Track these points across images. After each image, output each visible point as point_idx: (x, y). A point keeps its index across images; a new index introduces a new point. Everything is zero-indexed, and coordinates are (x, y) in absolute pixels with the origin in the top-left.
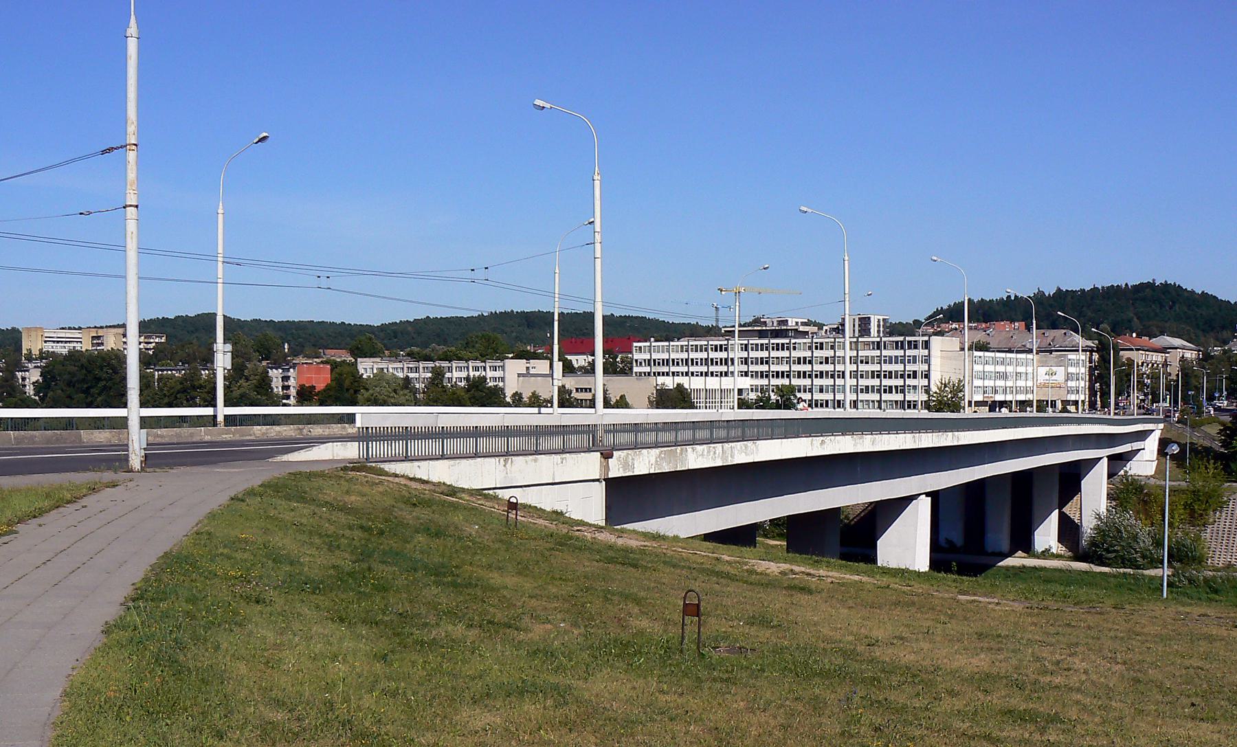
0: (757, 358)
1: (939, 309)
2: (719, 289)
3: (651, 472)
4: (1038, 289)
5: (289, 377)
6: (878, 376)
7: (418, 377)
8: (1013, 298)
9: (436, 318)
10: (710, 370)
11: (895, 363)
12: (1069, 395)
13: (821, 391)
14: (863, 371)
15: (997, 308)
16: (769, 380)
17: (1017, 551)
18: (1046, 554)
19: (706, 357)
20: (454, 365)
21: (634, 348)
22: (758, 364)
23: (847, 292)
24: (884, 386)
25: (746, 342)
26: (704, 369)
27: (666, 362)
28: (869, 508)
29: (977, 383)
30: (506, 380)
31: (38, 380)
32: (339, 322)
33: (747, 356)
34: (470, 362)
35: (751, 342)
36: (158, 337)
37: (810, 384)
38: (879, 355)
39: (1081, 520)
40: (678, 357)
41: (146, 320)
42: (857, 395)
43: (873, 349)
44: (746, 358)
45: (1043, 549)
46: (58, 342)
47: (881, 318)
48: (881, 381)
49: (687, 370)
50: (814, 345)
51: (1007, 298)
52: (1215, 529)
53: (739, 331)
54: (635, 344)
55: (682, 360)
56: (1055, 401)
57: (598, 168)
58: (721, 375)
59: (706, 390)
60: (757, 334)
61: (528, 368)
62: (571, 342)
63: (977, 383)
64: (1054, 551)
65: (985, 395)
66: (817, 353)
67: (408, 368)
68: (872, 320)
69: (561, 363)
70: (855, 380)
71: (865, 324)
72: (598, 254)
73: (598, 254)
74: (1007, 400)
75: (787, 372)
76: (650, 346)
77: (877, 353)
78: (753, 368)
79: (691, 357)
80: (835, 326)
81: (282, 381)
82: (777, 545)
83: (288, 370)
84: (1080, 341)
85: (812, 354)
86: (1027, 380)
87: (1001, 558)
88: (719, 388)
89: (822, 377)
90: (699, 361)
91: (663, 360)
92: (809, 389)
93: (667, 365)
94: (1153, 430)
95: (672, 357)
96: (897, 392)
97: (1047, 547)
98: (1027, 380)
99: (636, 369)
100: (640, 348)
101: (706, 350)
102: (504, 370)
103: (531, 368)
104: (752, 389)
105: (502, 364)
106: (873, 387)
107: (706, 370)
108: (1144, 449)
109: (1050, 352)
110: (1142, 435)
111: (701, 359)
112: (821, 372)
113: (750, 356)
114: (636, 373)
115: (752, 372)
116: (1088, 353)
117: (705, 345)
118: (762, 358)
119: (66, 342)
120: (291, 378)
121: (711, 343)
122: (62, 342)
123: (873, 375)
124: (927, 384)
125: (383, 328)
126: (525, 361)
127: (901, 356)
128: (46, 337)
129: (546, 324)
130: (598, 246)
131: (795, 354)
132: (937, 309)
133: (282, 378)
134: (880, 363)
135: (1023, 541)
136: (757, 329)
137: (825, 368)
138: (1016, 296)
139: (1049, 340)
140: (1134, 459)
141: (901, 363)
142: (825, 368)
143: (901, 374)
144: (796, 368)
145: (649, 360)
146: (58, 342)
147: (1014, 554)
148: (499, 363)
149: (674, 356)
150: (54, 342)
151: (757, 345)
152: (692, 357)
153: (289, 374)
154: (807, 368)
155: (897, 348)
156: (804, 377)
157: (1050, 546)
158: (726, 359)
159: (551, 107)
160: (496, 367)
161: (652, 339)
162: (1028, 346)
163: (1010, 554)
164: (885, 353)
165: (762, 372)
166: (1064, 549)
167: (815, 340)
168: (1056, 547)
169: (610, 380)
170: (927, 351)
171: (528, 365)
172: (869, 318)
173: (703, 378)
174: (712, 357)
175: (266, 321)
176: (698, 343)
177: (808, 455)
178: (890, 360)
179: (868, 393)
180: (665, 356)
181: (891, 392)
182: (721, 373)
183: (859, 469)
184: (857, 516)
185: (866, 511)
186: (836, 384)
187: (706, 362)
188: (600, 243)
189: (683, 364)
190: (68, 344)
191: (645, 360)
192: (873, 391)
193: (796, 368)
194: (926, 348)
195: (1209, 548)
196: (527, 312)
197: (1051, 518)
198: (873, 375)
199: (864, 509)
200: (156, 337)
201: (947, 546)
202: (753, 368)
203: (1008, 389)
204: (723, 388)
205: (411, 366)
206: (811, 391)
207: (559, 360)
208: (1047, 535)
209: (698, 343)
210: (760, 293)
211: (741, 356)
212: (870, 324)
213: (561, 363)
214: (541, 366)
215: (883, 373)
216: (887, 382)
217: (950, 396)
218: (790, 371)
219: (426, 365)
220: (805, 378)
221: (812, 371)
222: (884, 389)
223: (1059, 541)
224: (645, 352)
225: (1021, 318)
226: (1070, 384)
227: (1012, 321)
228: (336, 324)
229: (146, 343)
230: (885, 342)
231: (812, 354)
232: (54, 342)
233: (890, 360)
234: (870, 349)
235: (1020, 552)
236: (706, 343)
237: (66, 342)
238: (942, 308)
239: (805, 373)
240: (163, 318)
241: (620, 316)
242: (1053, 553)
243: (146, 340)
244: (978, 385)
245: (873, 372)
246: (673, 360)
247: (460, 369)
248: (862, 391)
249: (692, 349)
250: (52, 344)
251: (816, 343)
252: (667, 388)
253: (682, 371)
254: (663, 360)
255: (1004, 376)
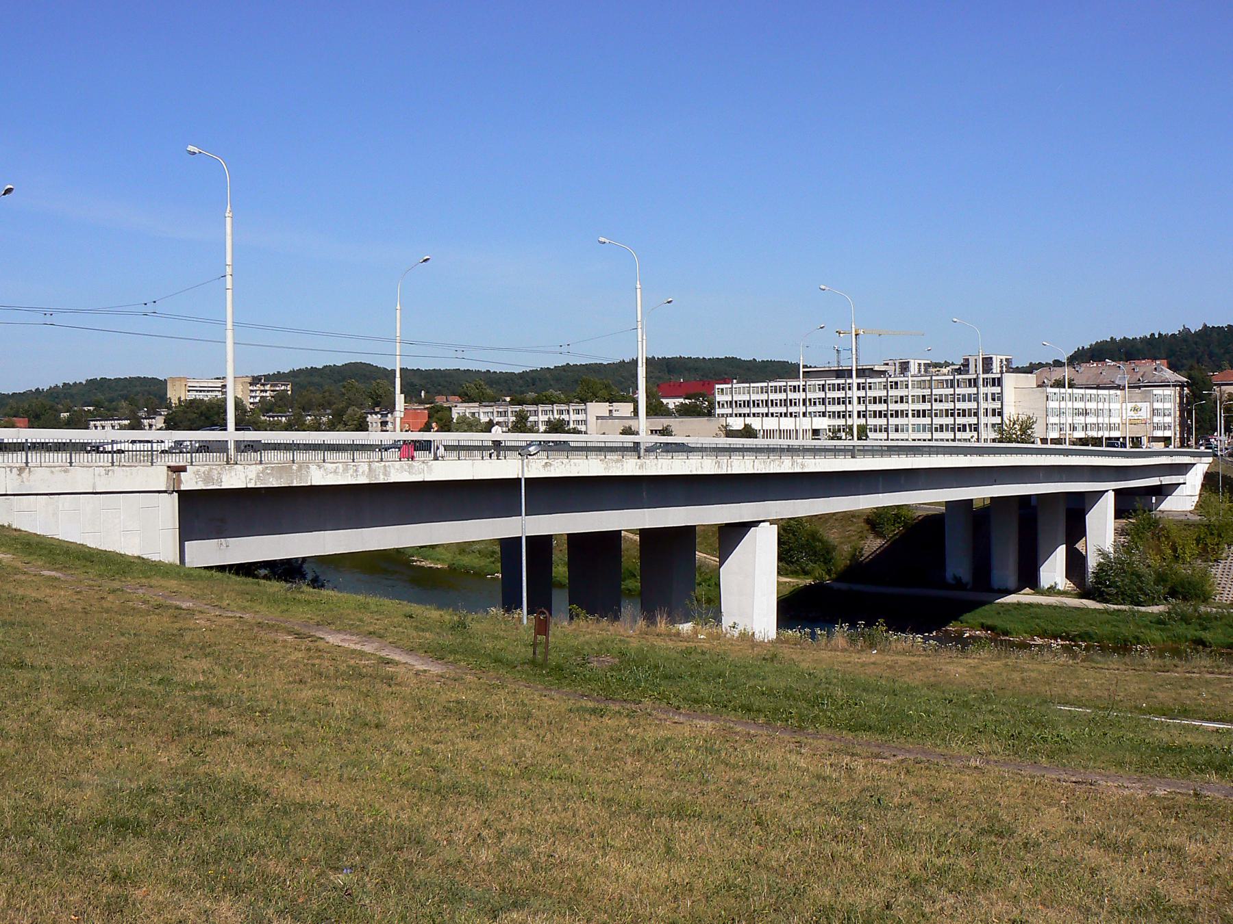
0: (834, 399)
1: (1081, 348)
2: (837, 332)
3: (249, 486)
4: (1184, 326)
5: (387, 422)
6: (952, 415)
7: (537, 420)
8: (1157, 336)
9: (576, 365)
10: (789, 411)
11: (968, 401)
12: (1155, 432)
13: (897, 430)
14: (937, 410)
15: (1140, 346)
16: (846, 420)
17: (1025, 588)
18: (1052, 591)
19: (785, 398)
20: (540, 409)
21: (716, 390)
22: (835, 404)
23: (639, 320)
24: (958, 425)
25: (823, 382)
26: (783, 410)
27: (747, 404)
28: (886, 545)
29: (1053, 420)
30: (588, 422)
31: (162, 427)
32: (484, 370)
33: (824, 396)
34: (555, 406)
35: (828, 382)
36: (284, 385)
37: (886, 423)
38: (953, 393)
39: (1086, 552)
40: (758, 399)
41: (295, 370)
42: (932, 433)
43: (947, 387)
44: (823, 399)
45: (1049, 586)
46: (201, 391)
47: (1004, 358)
48: (955, 419)
49: (767, 412)
50: (889, 384)
51: (1151, 336)
52: (1228, 564)
53: (804, 372)
54: (717, 386)
55: (762, 401)
56: (1141, 438)
57: (231, 206)
58: (781, 416)
59: (780, 431)
60: (834, 374)
61: (611, 411)
62: (670, 386)
63: (1053, 420)
64: (1061, 587)
65: (1061, 432)
66: (892, 392)
67: (498, 412)
68: (994, 359)
69: (403, 395)
70: (930, 418)
71: (987, 364)
72: (229, 285)
73: (229, 285)
74: (1111, 436)
75: (863, 411)
76: (732, 388)
77: (951, 391)
78: (831, 408)
79: (770, 398)
80: (957, 367)
81: (381, 426)
82: (786, 582)
83: (386, 415)
84: (1169, 375)
85: (888, 393)
86: (1110, 416)
87: (1003, 595)
88: (794, 428)
89: (897, 416)
90: (778, 402)
91: (744, 402)
92: (885, 428)
93: (748, 406)
94: (1194, 464)
95: (753, 398)
96: (971, 431)
97: (1053, 584)
98: (1110, 416)
99: (718, 411)
100: (722, 389)
101: (785, 391)
102: (586, 413)
103: (614, 411)
104: (830, 429)
105: (584, 407)
106: (947, 425)
107: (785, 411)
108: (1185, 483)
109: (1139, 387)
110: (1183, 469)
111: (781, 400)
112: (897, 412)
113: (827, 397)
114: (718, 415)
115: (830, 412)
116: (1178, 388)
117: (784, 386)
118: (839, 398)
119: (208, 391)
120: (389, 423)
121: (789, 384)
122: (204, 391)
123: (948, 413)
124: (1000, 422)
125: (523, 375)
126: (608, 403)
127: (974, 394)
128: (190, 387)
129: (687, 370)
130: (229, 278)
131: (871, 393)
132: (1078, 349)
133: (381, 423)
134: (954, 401)
135: (1029, 578)
136: (861, 373)
137: (899, 407)
138: (1160, 334)
139: (1139, 376)
140: (1173, 494)
141: (974, 401)
142: (899, 407)
143: (974, 412)
144: (872, 407)
145: (731, 402)
146: (201, 391)
147: (1020, 591)
148: (582, 406)
149: (754, 397)
150: (197, 391)
151: (834, 385)
152: (810, 397)
153: (388, 419)
154: (883, 407)
155: (970, 386)
156: (880, 417)
157: (1055, 583)
158: (785, 400)
159: (200, 152)
160: (579, 410)
161: (735, 381)
162: (1117, 383)
163: (1016, 591)
164: (958, 391)
165: (839, 412)
166: (1072, 585)
167: (890, 380)
168: (1063, 583)
169: (682, 422)
170: (999, 388)
171: (611, 408)
172: (991, 358)
173: (760, 418)
174: (772, 398)
175: (413, 370)
176: (778, 384)
177: (475, 478)
178: (963, 398)
179: (943, 431)
180: (746, 398)
181: (965, 430)
182: (781, 414)
183: (644, 493)
184: (873, 553)
185: (882, 549)
186: (934, 423)
187: (785, 403)
188: (231, 275)
189: (763, 406)
190: (210, 393)
191: (727, 402)
192: (947, 430)
193: (872, 407)
194: (999, 385)
195: (1219, 584)
196: (668, 358)
197: (1056, 555)
198: (948, 413)
199: (881, 546)
200: (282, 385)
201: (954, 582)
202: (831, 408)
203: (1089, 426)
204: (782, 428)
205: (500, 410)
206: (886, 430)
207: (401, 393)
208: (1054, 570)
209: (778, 384)
210: (880, 335)
211: (819, 397)
212: (992, 364)
213: (403, 395)
214: (625, 409)
215: (956, 411)
216: (960, 420)
217: (1019, 433)
218: (866, 411)
219: (514, 410)
220: (881, 417)
221: (887, 411)
222: (958, 428)
223: (1066, 577)
224: (727, 394)
225: (1164, 356)
226: (1156, 419)
227: (1155, 359)
228: (481, 371)
229: (272, 391)
230: (958, 380)
231: (888, 393)
232: (197, 391)
233: (963, 398)
234: (943, 388)
235: (1028, 588)
236: (785, 384)
237: (208, 391)
238: (1083, 347)
239: (880, 412)
240: (312, 367)
241: (763, 361)
242: (1059, 590)
243: (272, 389)
244: (1054, 422)
245: (947, 410)
246: (754, 401)
247: (545, 412)
248: (936, 430)
249: (771, 390)
250: (195, 393)
251: (891, 382)
252: (731, 428)
253: (763, 412)
254: (744, 402)
255: (1086, 413)
